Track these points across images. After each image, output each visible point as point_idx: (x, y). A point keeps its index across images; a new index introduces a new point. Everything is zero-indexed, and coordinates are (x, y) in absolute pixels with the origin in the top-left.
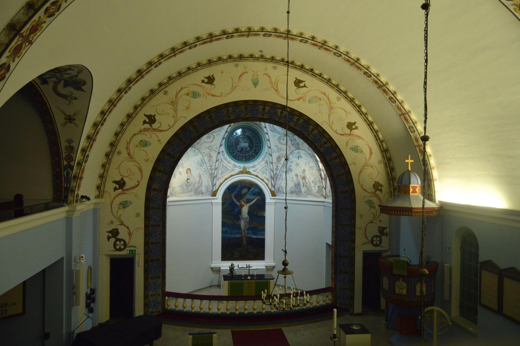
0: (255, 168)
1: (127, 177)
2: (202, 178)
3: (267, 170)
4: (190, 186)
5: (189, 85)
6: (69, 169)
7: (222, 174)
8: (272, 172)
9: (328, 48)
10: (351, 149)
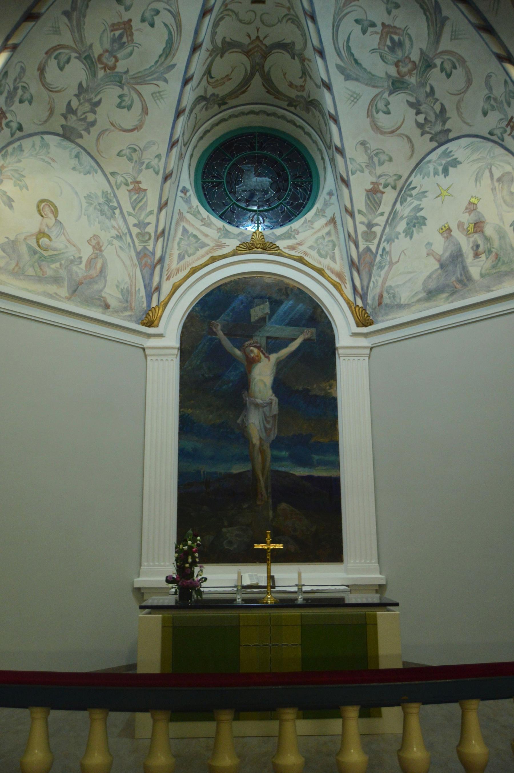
0: (295, 238)
2: (104, 253)
3: (334, 246)
4: (54, 262)
7: (181, 257)
8: (352, 246)
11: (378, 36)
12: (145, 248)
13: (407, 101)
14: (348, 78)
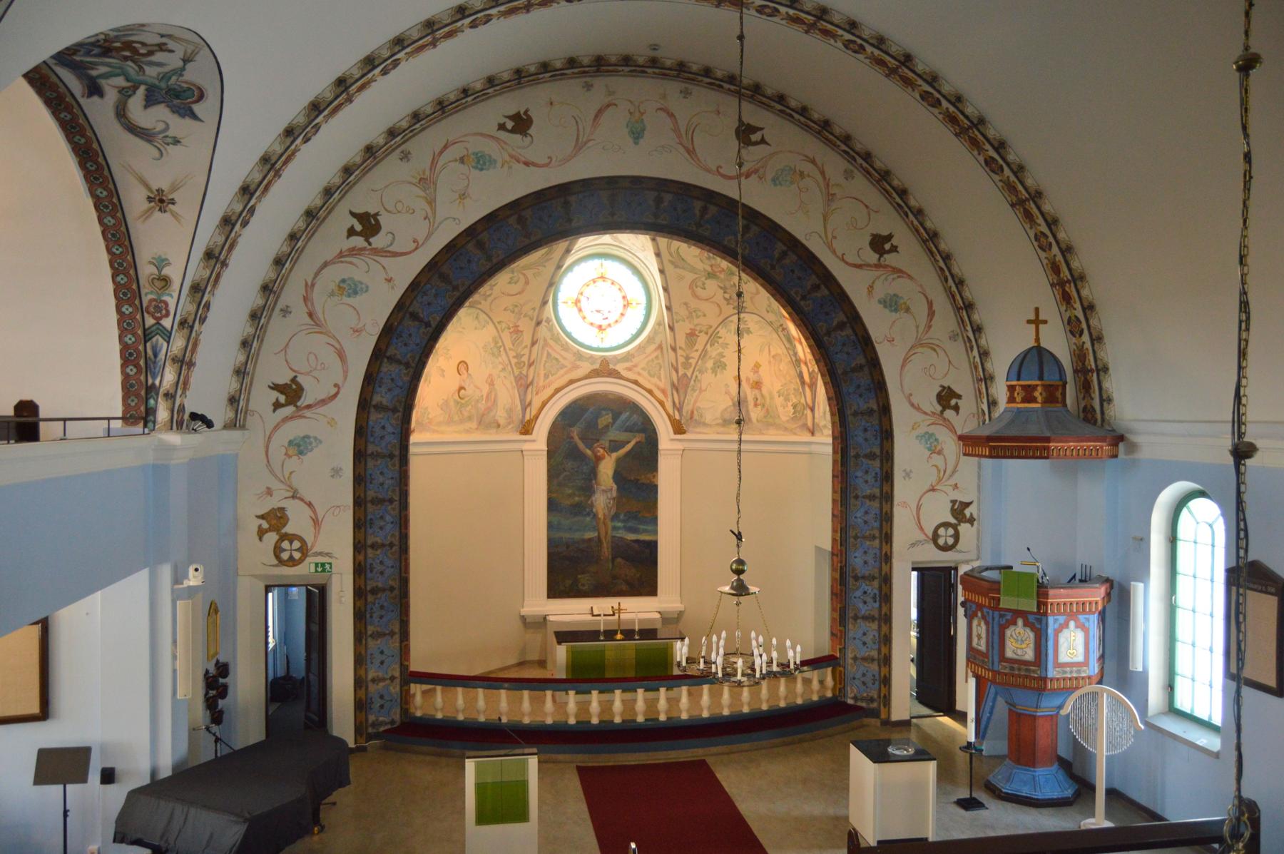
0: (632, 362)
1: (307, 374)
2: (496, 386)
3: (661, 367)
5: (465, 135)
6: (158, 336)
7: (546, 376)
8: (674, 373)
9: (829, 27)
10: (880, 302)
12: (521, 373)
14: (676, 266)
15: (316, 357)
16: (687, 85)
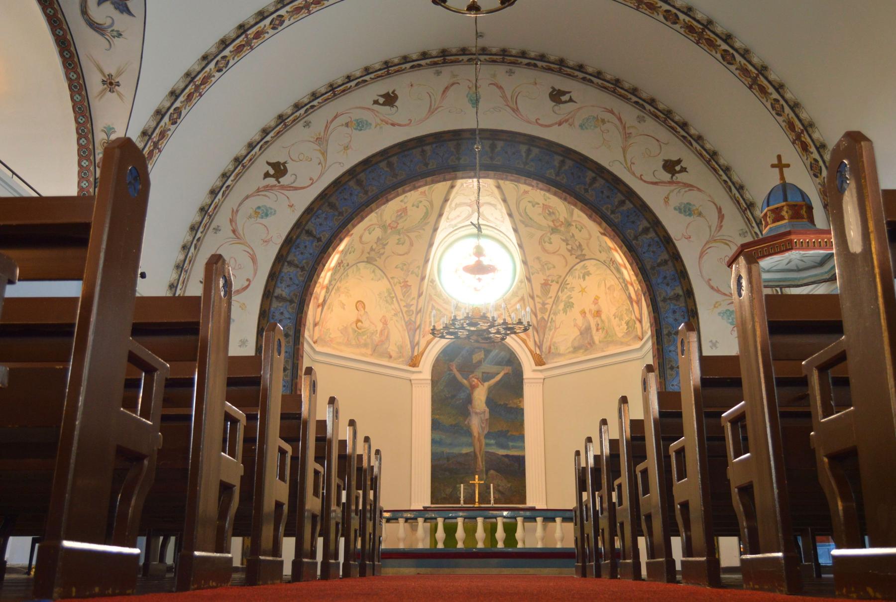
5: (350, 109)
8: (533, 317)
10: (675, 209)
11: (541, 209)
13: (561, 239)
14: (526, 226)
15: (235, 261)
16: (511, 68)
